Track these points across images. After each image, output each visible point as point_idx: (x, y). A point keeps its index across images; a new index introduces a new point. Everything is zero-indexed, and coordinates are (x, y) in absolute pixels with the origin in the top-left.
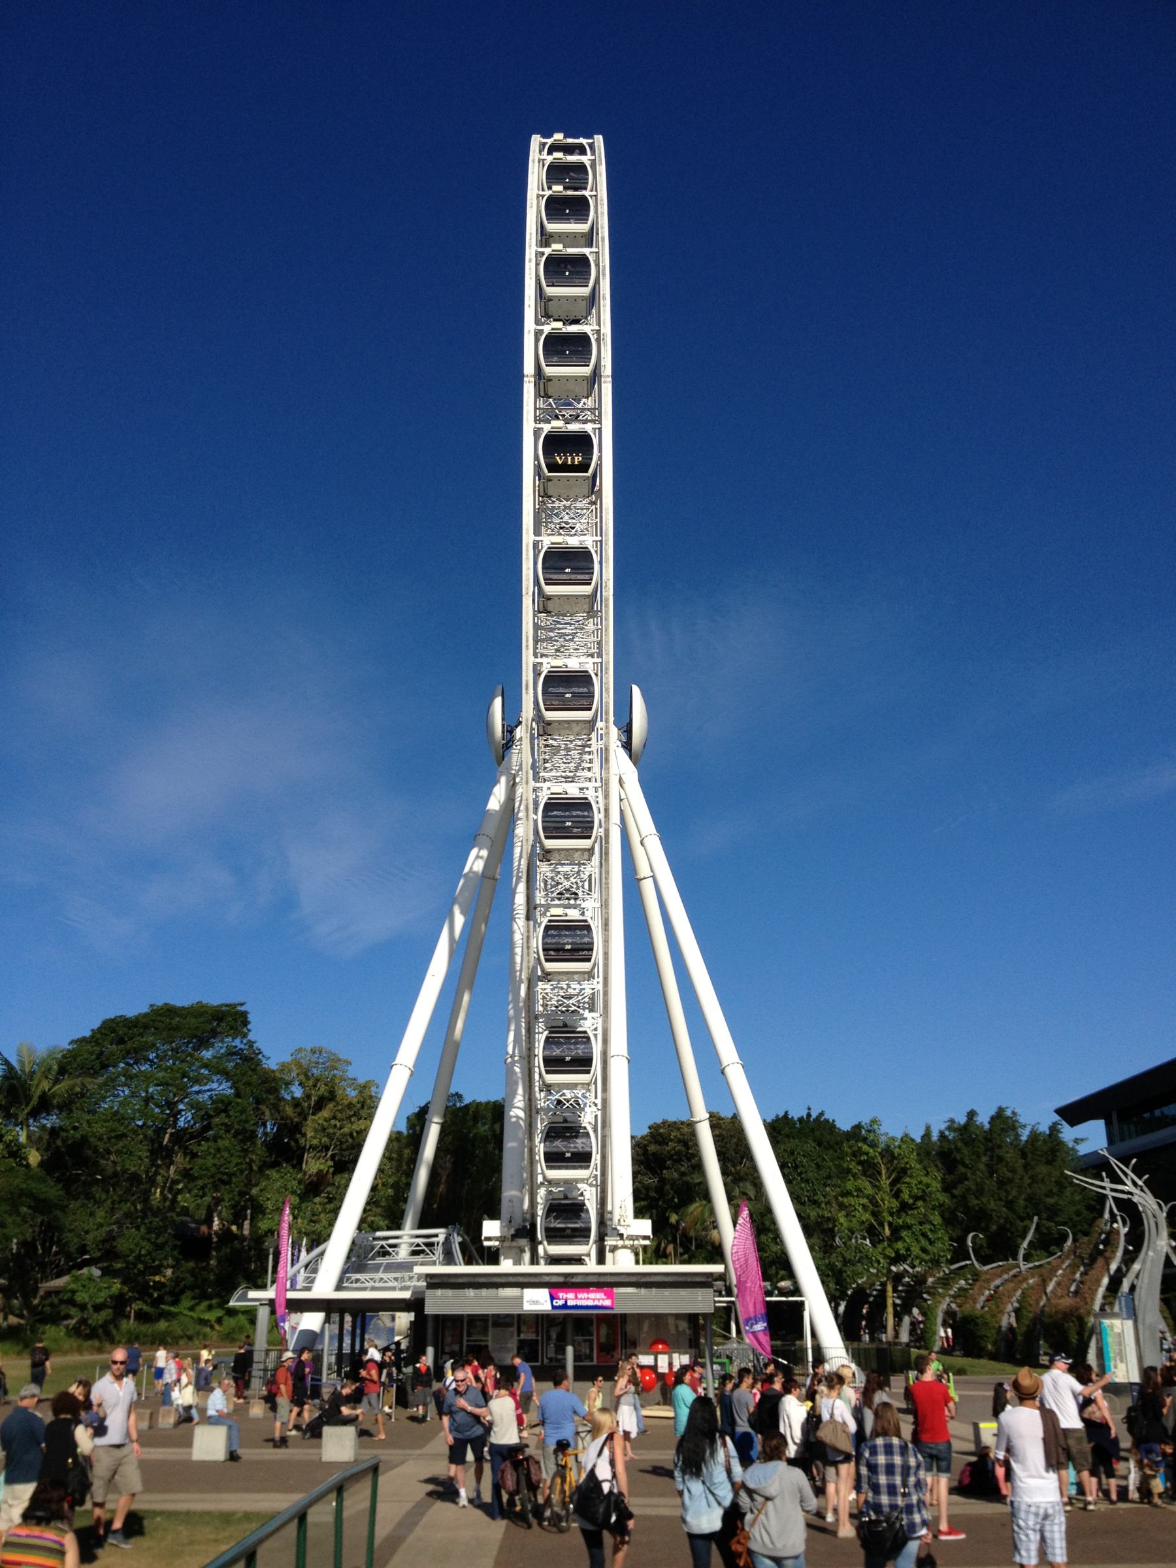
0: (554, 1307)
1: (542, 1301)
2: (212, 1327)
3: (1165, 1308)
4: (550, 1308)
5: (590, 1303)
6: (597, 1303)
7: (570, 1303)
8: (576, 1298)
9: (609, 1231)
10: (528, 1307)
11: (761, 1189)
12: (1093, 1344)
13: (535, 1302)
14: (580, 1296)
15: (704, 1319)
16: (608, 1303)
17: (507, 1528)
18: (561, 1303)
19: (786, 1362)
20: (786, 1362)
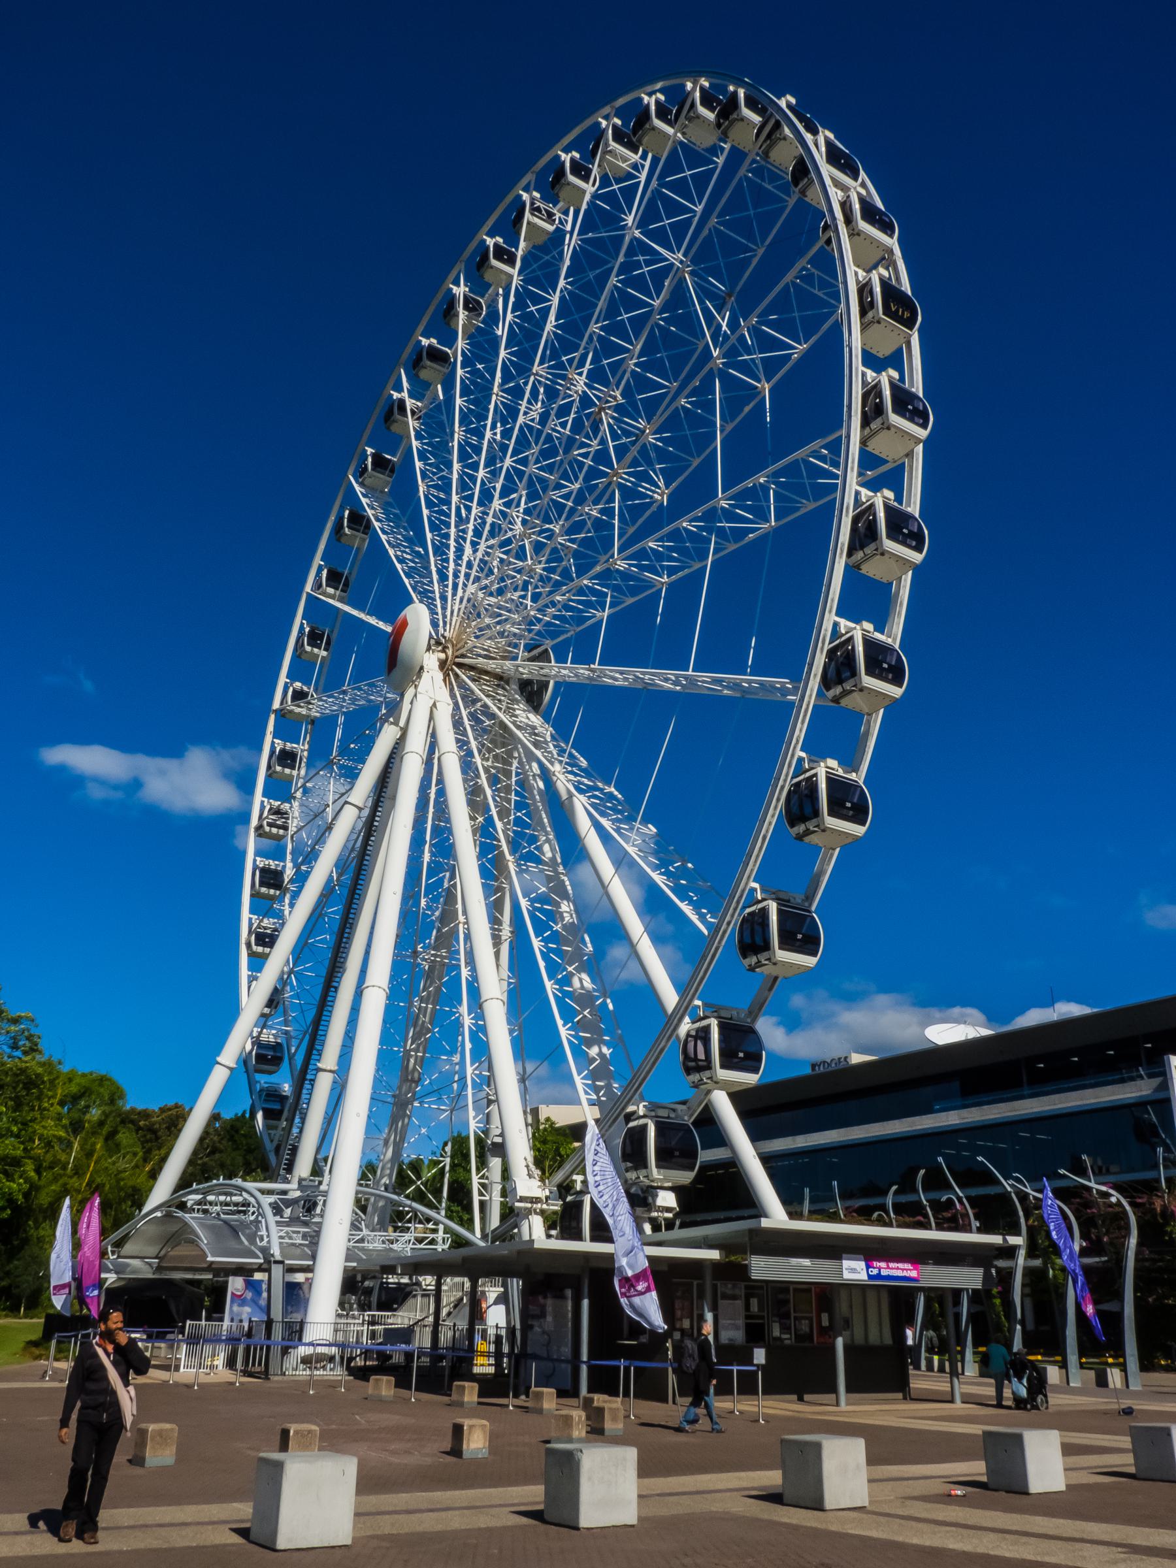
0: (870, 1277)
1: (859, 1270)
2: (48, 1110)
3: (802, 970)
4: (866, 1278)
5: (899, 1273)
6: (905, 1274)
7: (884, 1273)
8: (888, 1268)
9: (503, 1250)
10: (847, 1275)
11: (829, 1217)
12: (101, 1307)
13: (853, 1270)
14: (891, 1265)
15: (468, 1219)
16: (914, 1274)
17: (104, 1508)
18: (875, 1272)
19: (589, 1035)
20: (589, 1035)
